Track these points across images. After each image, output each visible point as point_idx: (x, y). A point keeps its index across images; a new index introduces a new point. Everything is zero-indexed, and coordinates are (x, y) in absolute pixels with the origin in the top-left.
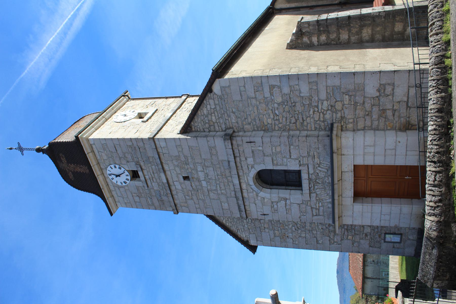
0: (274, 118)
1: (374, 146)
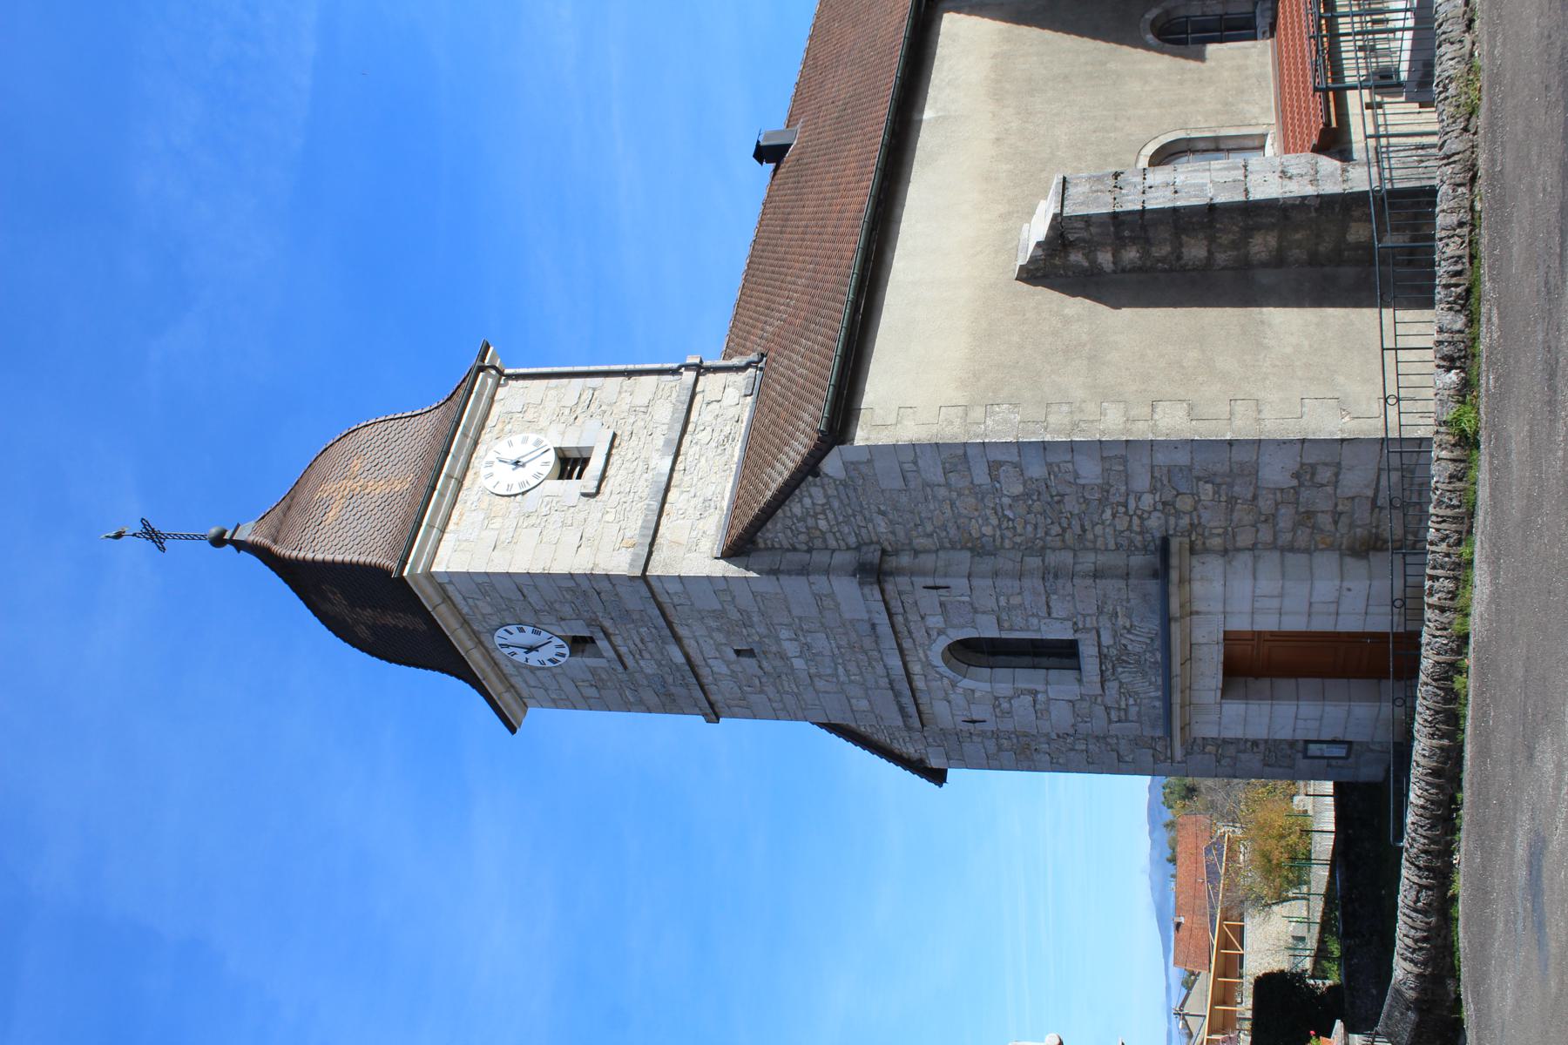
0: (999, 526)
1: (1281, 596)
